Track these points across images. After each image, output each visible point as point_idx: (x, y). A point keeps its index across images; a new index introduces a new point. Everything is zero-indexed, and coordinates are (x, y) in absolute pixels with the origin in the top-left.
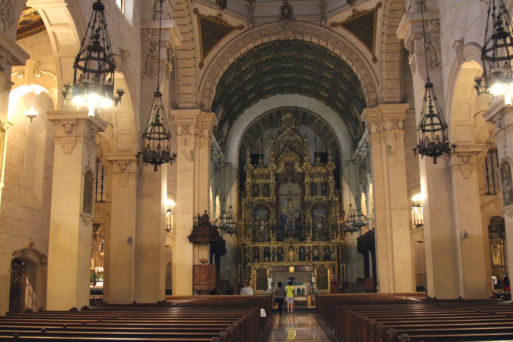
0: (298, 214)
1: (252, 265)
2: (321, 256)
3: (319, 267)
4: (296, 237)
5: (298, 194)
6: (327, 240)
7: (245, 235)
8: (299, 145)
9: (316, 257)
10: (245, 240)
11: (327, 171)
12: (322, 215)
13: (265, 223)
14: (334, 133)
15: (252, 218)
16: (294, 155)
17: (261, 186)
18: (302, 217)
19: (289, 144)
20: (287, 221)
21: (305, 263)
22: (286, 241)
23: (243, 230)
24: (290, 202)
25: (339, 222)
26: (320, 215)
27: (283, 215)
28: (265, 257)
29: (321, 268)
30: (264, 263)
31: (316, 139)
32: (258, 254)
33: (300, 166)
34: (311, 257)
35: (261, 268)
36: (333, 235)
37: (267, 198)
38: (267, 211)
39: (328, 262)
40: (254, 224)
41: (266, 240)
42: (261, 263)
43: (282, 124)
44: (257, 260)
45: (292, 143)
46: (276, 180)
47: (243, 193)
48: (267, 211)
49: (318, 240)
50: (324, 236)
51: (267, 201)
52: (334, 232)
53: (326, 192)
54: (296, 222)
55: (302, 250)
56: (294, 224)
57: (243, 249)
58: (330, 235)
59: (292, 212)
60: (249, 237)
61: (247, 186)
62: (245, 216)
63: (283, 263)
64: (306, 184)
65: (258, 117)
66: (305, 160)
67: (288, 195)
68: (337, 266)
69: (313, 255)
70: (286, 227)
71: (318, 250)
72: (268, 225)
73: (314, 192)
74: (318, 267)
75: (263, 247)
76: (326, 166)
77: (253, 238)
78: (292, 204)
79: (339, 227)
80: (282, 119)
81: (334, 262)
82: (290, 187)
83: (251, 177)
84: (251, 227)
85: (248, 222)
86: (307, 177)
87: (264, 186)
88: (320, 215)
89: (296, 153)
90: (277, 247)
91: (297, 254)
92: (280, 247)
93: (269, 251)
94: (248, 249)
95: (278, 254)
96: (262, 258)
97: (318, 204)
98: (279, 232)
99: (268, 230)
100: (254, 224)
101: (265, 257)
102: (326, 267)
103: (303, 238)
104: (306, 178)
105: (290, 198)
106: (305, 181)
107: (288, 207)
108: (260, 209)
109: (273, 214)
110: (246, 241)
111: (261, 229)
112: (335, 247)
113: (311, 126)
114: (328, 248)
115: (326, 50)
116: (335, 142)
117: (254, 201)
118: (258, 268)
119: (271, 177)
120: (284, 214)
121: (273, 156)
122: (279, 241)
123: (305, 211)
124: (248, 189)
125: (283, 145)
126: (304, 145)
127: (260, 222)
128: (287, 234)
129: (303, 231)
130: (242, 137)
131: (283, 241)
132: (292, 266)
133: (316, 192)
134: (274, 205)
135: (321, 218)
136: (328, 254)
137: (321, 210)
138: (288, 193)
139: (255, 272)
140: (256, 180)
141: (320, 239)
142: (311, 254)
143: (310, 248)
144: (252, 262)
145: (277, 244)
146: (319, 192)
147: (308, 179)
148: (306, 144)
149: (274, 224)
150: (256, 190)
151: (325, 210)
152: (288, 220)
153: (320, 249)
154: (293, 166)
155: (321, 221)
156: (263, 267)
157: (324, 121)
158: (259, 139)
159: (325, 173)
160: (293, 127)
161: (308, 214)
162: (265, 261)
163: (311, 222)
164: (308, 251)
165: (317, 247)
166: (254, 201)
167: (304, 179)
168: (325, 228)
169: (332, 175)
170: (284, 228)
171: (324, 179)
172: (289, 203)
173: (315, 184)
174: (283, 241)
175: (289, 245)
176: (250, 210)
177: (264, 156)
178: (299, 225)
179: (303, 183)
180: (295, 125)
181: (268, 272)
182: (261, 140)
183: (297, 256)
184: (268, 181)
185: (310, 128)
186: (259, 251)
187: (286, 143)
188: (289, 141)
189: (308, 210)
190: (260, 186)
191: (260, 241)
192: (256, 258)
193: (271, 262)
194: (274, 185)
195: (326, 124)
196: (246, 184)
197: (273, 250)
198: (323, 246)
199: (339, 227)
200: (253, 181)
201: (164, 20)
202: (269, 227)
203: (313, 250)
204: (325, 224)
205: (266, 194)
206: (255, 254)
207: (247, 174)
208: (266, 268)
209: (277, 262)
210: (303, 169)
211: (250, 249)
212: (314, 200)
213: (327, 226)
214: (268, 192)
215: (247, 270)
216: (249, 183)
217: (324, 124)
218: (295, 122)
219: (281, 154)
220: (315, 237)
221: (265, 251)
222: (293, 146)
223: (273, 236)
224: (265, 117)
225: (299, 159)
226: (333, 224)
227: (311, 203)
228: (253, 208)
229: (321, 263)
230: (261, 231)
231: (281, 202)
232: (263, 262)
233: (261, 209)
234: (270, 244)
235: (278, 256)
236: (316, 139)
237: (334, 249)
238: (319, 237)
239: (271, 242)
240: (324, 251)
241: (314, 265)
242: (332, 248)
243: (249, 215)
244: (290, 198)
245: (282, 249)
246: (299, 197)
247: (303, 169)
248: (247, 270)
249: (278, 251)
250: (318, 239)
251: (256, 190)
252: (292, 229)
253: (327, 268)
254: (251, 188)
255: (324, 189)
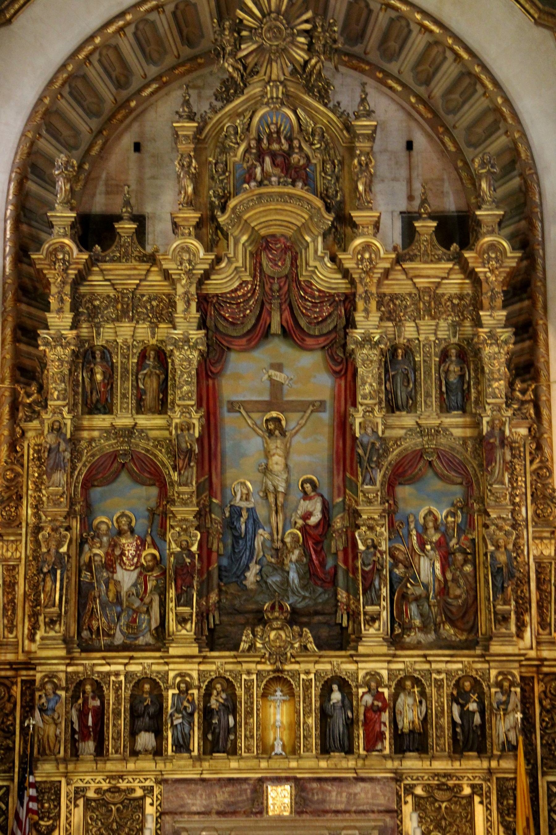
0: (319, 507)
1: (66, 775)
2: (440, 727)
3: (426, 787)
4: (302, 625)
5: (320, 406)
6: (469, 645)
7: (35, 615)
8: (326, 150)
9: (412, 732)
10: (32, 639)
11: (468, 290)
12: (441, 513)
13: (142, 545)
14: (507, 101)
15: (76, 525)
16: (300, 199)
17: (126, 356)
18: (338, 523)
19: (275, 146)
20: (258, 542)
21: (351, 764)
22: (252, 647)
23: (21, 588)
24: (276, 446)
25: (534, 552)
26: (430, 512)
27: (236, 512)
28: (133, 734)
29: (438, 795)
30: (131, 766)
31: (409, 145)
32: (100, 713)
33: (333, 259)
34: (381, 736)
35: (115, 790)
36: (505, 619)
37: (159, 421)
38: (154, 491)
39: (476, 763)
40: (85, 558)
41: (146, 639)
42: (109, 766)
43: (241, 40)
44: (90, 745)
45: (290, 140)
46: (202, 324)
47: (29, 395)
48: (154, 491)
49: (418, 646)
50: (453, 624)
51: (153, 434)
52: (506, 602)
53: (466, 395)
54: (305, 546)
55: (336, 696)
56: (295, 555)
57: (17, 691)
58: (482, 618)
59: (286, 494)
60: (51, 623)
61: (51, 355)
62: (36, 515)
63: (234, 764)
64: (361, 345)
65: (122, 15)
66: (355, 225)
67: (269, 406)
68: (523, 782)
69: (394, 721)
70: (251, 576)
71: (423, 693)
72: (158, 562)
73: (401, 395)
74: (419, 791)
75: (127, 675)
76: (467, 255)
77: (73, 628)
78: (287, 455)
79: (533, 575)
80: (241, 14)
81: (507, 764)
82: (279, 367)
83: (74, 308)
84: (64, 569)
85: (47, 541)
86: (367, 311)
87: (143, 356)
88: (430, 512)
89: (315, 192)
90: (201, 674)
91: (307, 713)
92: (221, 678)
93: (159, 699)
94: (43, 686)
95: (208, 713)
96: (117, 739)
97: (420, 454)
98: (214, 597)
99: (156, 587)
100: (85, 558)
101: (133, 734)
102: (467, 791)
103: (344, 630)
104: (359, 316)
105: (277, 420)
106: (357, 334)
107: (266, 470)
108: (117, 475)
109: (185, 503)
110: (34, 647)
111: (117, 583)
112: (512, 684)
113: (388, 75)
114: (476, 684)
115: (306, 250)
116: (513, 149)
117: (85, 434)
118: (98, 791)
119: (180, 306)
120: (244, 504)
121: (190, 204)
122: (212, 650)
123: (355, 490)
124: (53, 369)
125: (247, 150)
126: (351, 150)
127: (114, 545)
128: (260, 611)
129: (342, 595)
130: (34, 110)
131: (236, 647)
132: (278, 781)
133: (412, 397)
134: (190, 451)
135: (436, 528)
136: (477, 719)
137: (437, 485)
138: (266, 397)
139: (78, 814)
140: (98, 326)
141: (432, 637)
142: (385, 717)
143: (380, 684)
144: (65, 761)
145: (205, 660)
146: (428, 395)
147: (375, 317)
148: (362, 145)
149: (191, 555)
150: (99, 377)
151: (457, 489)
152: (262, 535)
153: (432, 691)
154: (294, 259)
155: (438, 546)
156: (123, 785)
157: (458, 39)
158: (127, 141)
159: (461, 297)
160: (300, 55)
161: (370, 502)
162: (135, 753)
163: (384, 547)
164: (368, 699)
165: (417, 682)
166: (85, 434)
167: (351, 323)
168: (455, 580)
169: (499, 301)
170: (241, 576)
171: (455, 326)
172: (272, 446)
173: (409, 351)
174: (236, 647)
175: (268, 667)
176: (60, 477)
177: (149, 227)
178: (323, 564)
179: (344, 346)
180: (310, 49)
181: (150, 810)
182: (137, 147)
183: (307, 728)
184: (163, 329)
185: (382, 82)
186: (102, 698)
187: (259, 141)
188: (278, 132)
189: (372, 482)
190: (117, 360)
191: (110, 648)
192: (85, 738)
193: (167, 759)
194: (194, 347)
195: (465, 56)
196: (47, 344)
197: (184, 693)
198: (448, 673)
199: (533, 575)
200: (85, 331)
201: (21, 534)
202: (164, 573)
203: (395, 697)
204: (460, 557)
205: (149, 399)
206: (82, 715)
207: (54, 290)
208: (139, 793)
209: (199, 759)
210: (346, 273)
211: (56, 687)
212: (402, 432)
213: (468, 568)
214: (163, 388)
215: (33, 806)
216: (62, 336)
217: (457, 56)
218: (306, 33)
219: (236, 194)
220: (407, 628)
221: (134, 699)
222: (295, 158)
223: (182, 620)
224: (153, 16)
225: (329, 218)
226: (502, 558)
227: (387, 451)
228: (82, 469)
229: (440, 765)
230: (118, 595)
231: (228, 444)
232: (124, 760)
233: (124, 478)
234: (167, 660)
235: (207, 726)
236: (409, 145)
237: (508, 693)
238: (424, 628)
239: (172, 651)
240: (454, 699)
241: (398, 777)
242: (499, 685)
243: (57, 504)
244: (277, 420)
245: (229, 686)
246: (325, 416)
247: (346, 273)
248: (33, 806)
249: (208, 695)
250: (421, 636)
251: (99, 377)
252: (286, 581)
253: (470, 798)
254: (73, 363)
255: (453, 378)
